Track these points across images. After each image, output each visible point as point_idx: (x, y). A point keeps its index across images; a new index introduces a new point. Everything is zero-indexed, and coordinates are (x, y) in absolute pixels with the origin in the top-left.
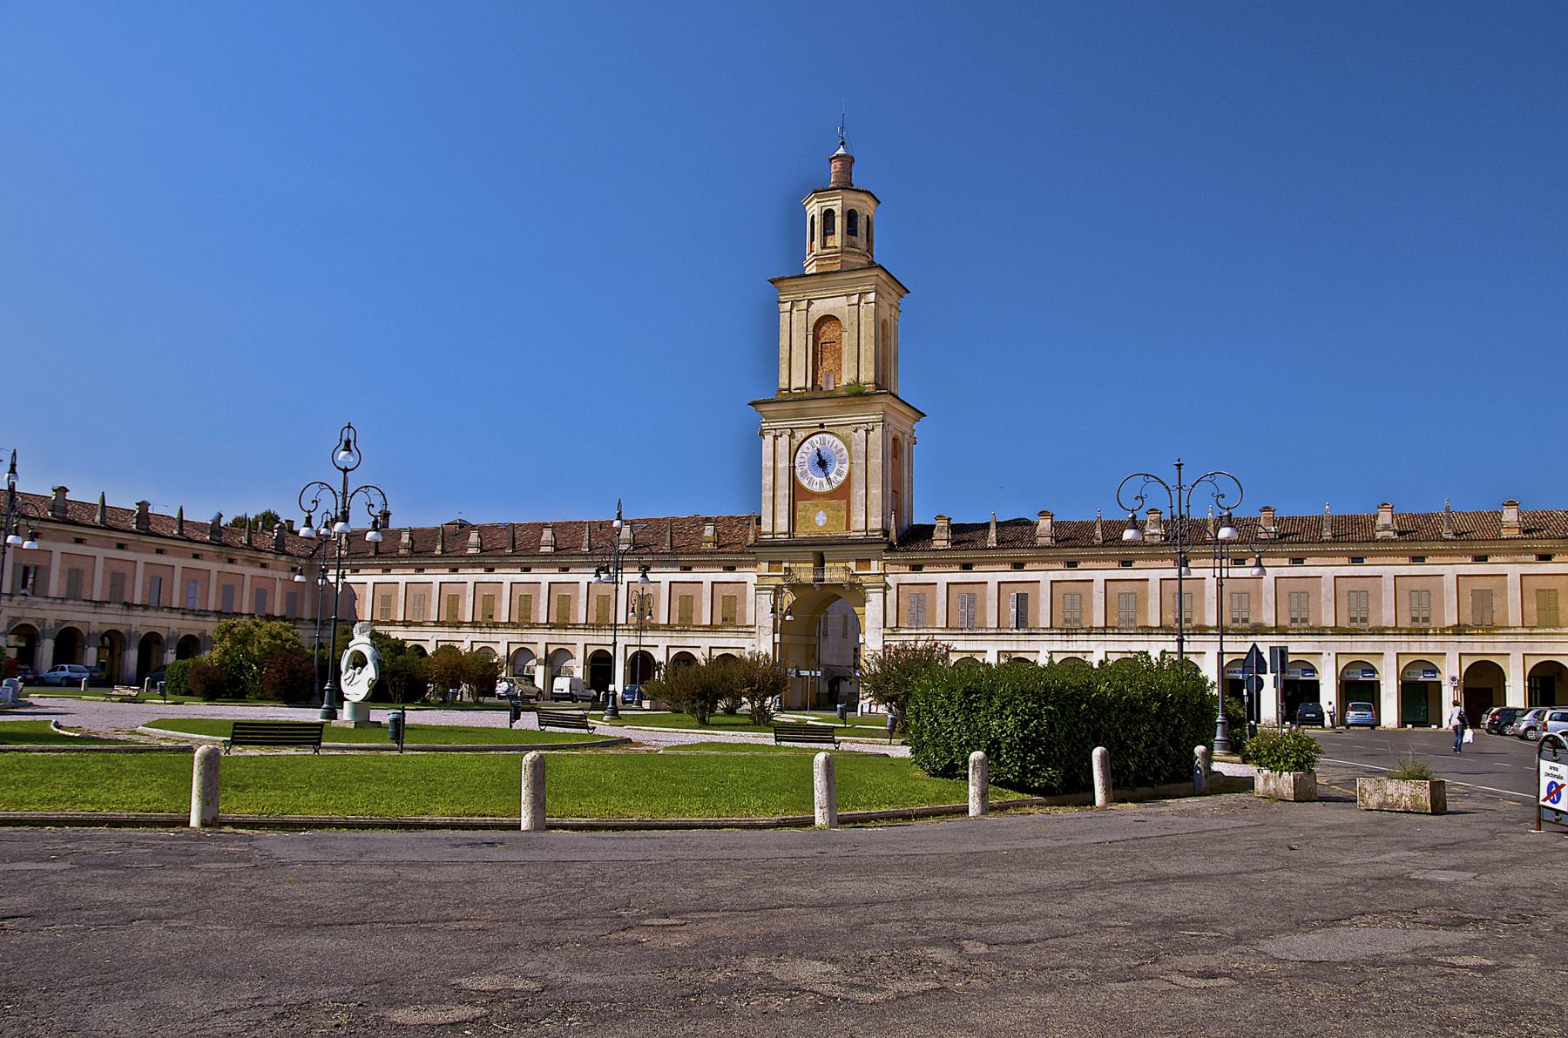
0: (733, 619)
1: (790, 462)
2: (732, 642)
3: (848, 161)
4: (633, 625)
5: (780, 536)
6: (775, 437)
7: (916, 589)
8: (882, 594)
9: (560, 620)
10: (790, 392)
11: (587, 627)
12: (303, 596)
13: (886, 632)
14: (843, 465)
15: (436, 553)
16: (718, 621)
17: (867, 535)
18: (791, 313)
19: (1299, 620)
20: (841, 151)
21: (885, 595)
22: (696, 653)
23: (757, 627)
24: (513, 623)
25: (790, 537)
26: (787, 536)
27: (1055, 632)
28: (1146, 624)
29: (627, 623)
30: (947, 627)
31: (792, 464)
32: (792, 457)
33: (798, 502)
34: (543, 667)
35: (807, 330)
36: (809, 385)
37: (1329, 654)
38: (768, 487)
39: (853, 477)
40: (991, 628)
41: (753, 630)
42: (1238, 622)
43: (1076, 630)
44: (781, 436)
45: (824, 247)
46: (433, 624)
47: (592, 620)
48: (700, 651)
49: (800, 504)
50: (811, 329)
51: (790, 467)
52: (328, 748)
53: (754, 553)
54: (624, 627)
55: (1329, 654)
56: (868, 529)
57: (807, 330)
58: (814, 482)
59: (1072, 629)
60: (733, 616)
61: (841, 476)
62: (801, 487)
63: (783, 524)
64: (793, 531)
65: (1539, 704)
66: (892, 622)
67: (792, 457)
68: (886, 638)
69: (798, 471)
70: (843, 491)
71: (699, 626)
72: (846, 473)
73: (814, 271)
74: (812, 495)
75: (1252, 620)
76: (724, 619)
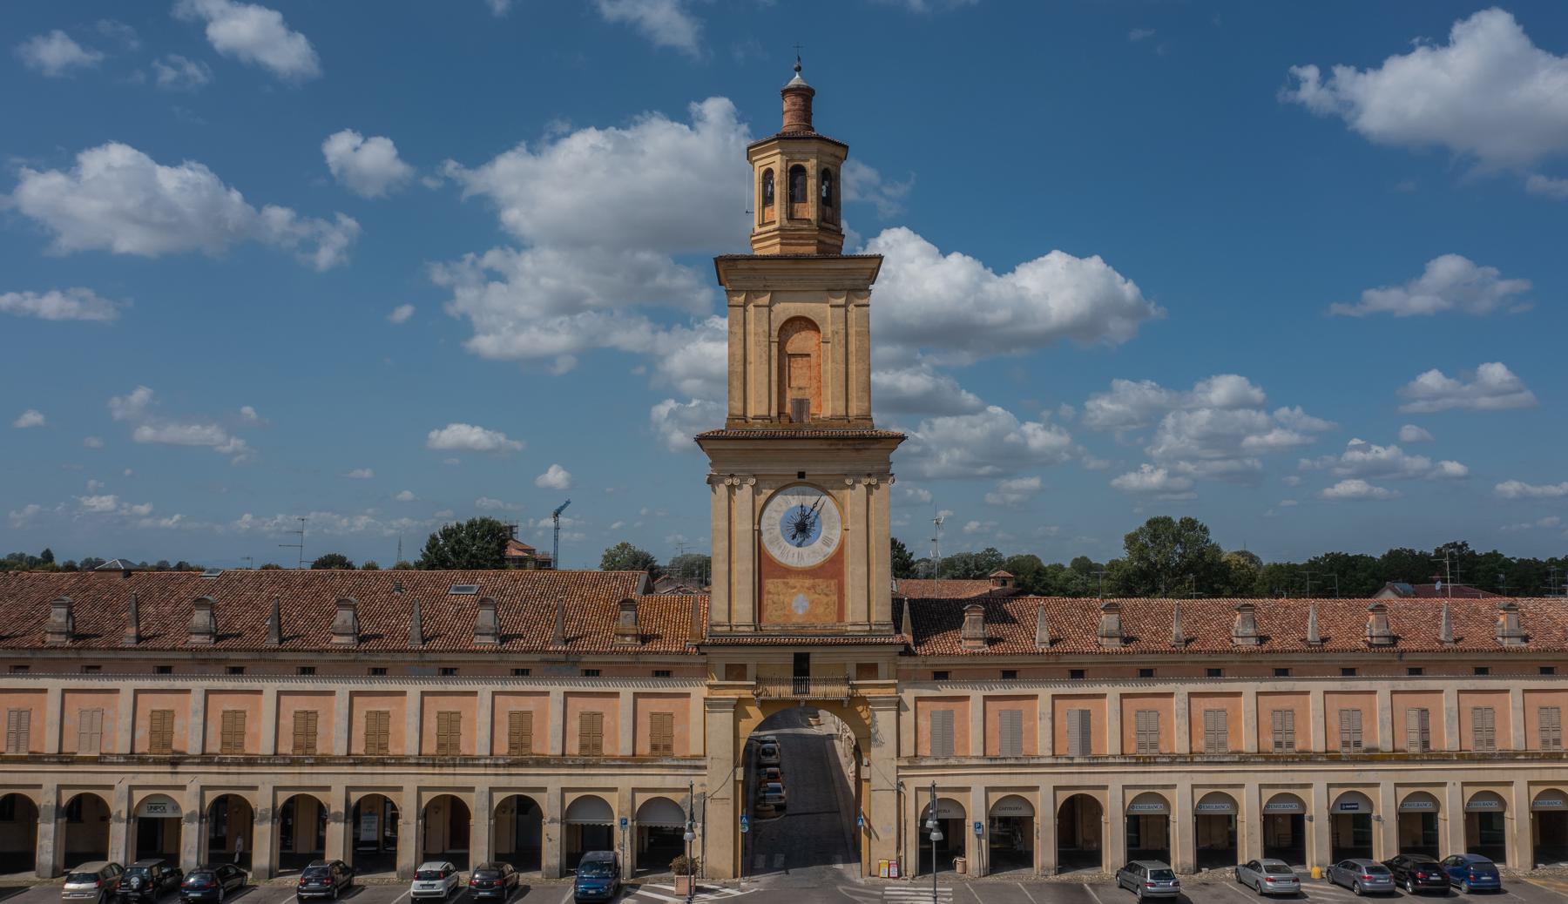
0: (668, 747)
1: (754, 525)
2: (670, 782)
3: (805, 95)
4: (503, 757)
5: (741, 629)
6: (731, 488)
7: (941, 706)
8: (894, 712)
9: (371, 750)
10: (746, 422)
11: (422, 761)
12: (1409, 661)
13: (901, 764)
14: (833, 532)
15: (125, 640)
16: (644, 748)
17: (871, 629)
18: (745, 310)
19: (1284, 746)
20: (796, 80)
21: (898, 715)
22: (613, 800)
23: (709, 758)
24: (284, 756)
25: (756, 630)
26: (753, 628)
27: (1128, 761)
28: (1239, 749)
29: (491, 754)
30: (985, 755)
31: (756, 527)
32: (757, 517)
33: (767, 581)
34: (343, 824)
35: (770, 336)
36: (774, 413)
37: (1454, 784)
38: (721, 558)
39: (848, 551)
40: (1043, 757)
41: (702, 763)
42: (1281, 747)
43: (1155, 758)
44: (740, 487)
45: (791, 217)
46: (55, 760)
47: (430, 748)
48: (616, 795)
49: (769, 584)
50: (775, 334)
51: (754, 530)
52: (812, 244)
53: (705, 654)
54: (488, 761)
55: (1454, 784)
56: (734, 622)
57: (770, 336)
58: (786, 553)
59: (1150, 757)
60: (667, 742)
61: (829, 546)
62: (771, 560)
63: (743, 612)
64: (760, 621)
65: (394, 849)
66: (907, 750)
67: (757, 517)
68: (901, 773)
69: (765, 538)
70: (832, 568)
71: (684, 759)
72: (836, 541)
73: (776, 250)
74: (785, 572)
75: (1365, 745)
76: (654, 747)
